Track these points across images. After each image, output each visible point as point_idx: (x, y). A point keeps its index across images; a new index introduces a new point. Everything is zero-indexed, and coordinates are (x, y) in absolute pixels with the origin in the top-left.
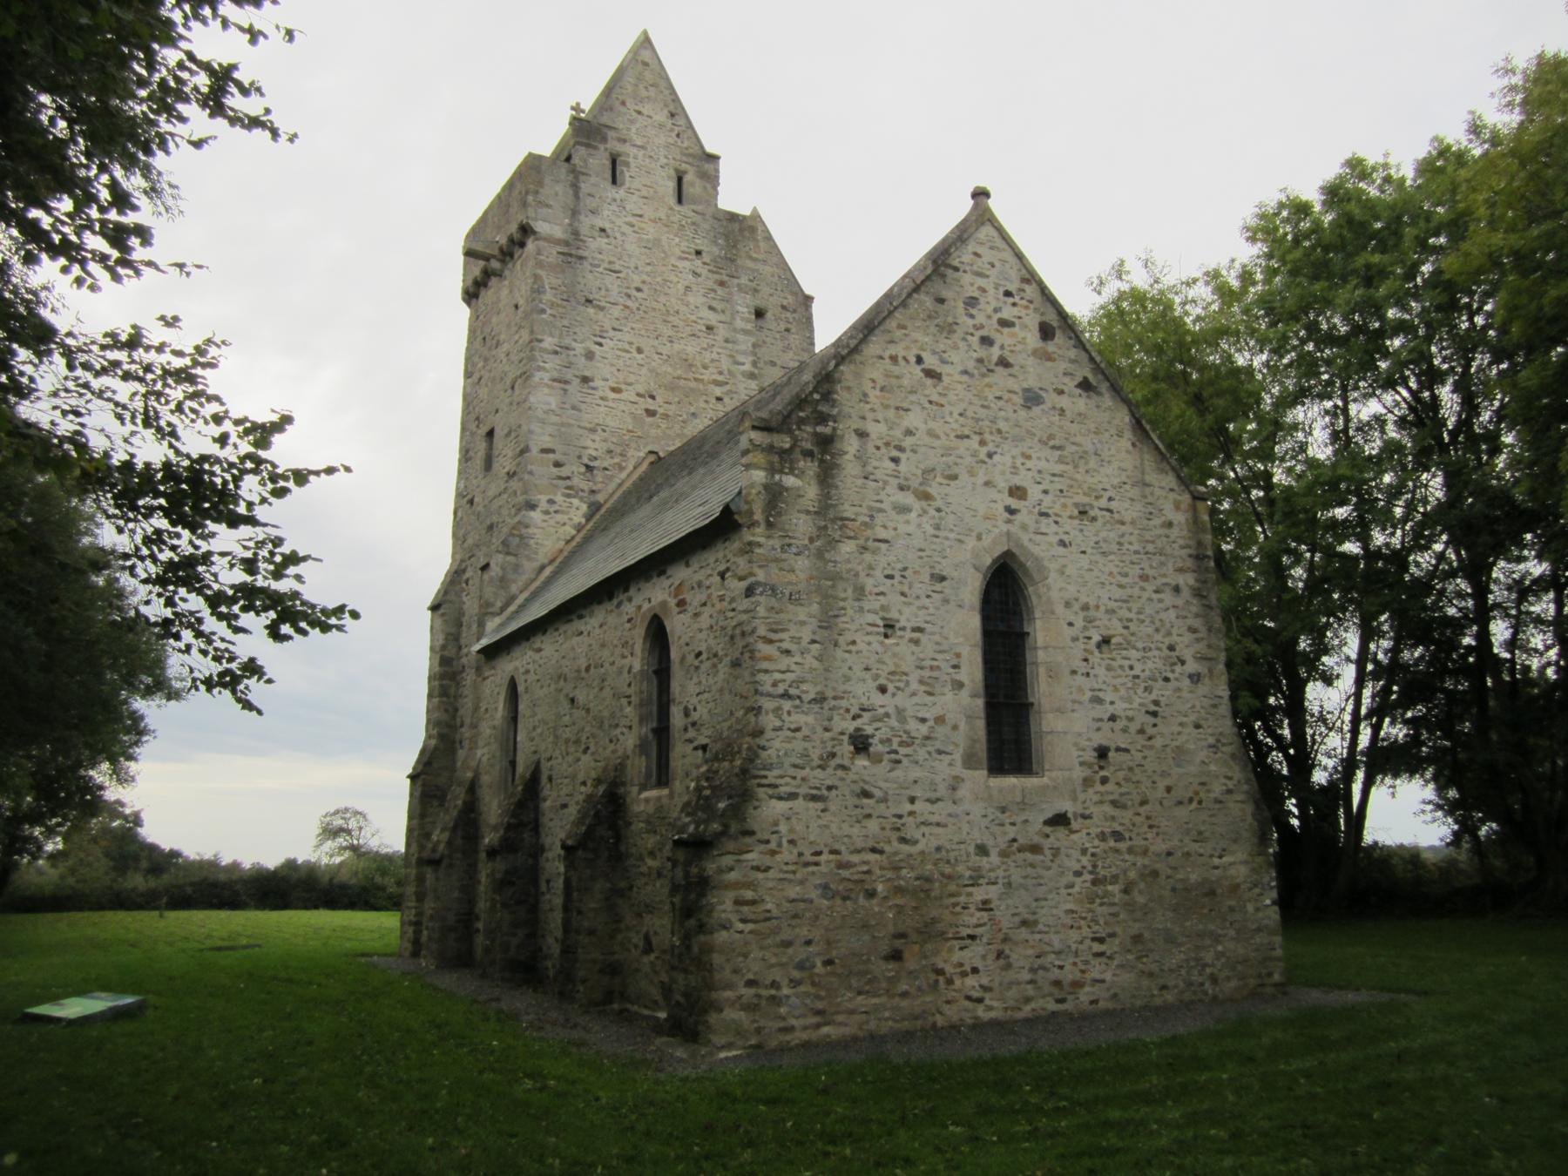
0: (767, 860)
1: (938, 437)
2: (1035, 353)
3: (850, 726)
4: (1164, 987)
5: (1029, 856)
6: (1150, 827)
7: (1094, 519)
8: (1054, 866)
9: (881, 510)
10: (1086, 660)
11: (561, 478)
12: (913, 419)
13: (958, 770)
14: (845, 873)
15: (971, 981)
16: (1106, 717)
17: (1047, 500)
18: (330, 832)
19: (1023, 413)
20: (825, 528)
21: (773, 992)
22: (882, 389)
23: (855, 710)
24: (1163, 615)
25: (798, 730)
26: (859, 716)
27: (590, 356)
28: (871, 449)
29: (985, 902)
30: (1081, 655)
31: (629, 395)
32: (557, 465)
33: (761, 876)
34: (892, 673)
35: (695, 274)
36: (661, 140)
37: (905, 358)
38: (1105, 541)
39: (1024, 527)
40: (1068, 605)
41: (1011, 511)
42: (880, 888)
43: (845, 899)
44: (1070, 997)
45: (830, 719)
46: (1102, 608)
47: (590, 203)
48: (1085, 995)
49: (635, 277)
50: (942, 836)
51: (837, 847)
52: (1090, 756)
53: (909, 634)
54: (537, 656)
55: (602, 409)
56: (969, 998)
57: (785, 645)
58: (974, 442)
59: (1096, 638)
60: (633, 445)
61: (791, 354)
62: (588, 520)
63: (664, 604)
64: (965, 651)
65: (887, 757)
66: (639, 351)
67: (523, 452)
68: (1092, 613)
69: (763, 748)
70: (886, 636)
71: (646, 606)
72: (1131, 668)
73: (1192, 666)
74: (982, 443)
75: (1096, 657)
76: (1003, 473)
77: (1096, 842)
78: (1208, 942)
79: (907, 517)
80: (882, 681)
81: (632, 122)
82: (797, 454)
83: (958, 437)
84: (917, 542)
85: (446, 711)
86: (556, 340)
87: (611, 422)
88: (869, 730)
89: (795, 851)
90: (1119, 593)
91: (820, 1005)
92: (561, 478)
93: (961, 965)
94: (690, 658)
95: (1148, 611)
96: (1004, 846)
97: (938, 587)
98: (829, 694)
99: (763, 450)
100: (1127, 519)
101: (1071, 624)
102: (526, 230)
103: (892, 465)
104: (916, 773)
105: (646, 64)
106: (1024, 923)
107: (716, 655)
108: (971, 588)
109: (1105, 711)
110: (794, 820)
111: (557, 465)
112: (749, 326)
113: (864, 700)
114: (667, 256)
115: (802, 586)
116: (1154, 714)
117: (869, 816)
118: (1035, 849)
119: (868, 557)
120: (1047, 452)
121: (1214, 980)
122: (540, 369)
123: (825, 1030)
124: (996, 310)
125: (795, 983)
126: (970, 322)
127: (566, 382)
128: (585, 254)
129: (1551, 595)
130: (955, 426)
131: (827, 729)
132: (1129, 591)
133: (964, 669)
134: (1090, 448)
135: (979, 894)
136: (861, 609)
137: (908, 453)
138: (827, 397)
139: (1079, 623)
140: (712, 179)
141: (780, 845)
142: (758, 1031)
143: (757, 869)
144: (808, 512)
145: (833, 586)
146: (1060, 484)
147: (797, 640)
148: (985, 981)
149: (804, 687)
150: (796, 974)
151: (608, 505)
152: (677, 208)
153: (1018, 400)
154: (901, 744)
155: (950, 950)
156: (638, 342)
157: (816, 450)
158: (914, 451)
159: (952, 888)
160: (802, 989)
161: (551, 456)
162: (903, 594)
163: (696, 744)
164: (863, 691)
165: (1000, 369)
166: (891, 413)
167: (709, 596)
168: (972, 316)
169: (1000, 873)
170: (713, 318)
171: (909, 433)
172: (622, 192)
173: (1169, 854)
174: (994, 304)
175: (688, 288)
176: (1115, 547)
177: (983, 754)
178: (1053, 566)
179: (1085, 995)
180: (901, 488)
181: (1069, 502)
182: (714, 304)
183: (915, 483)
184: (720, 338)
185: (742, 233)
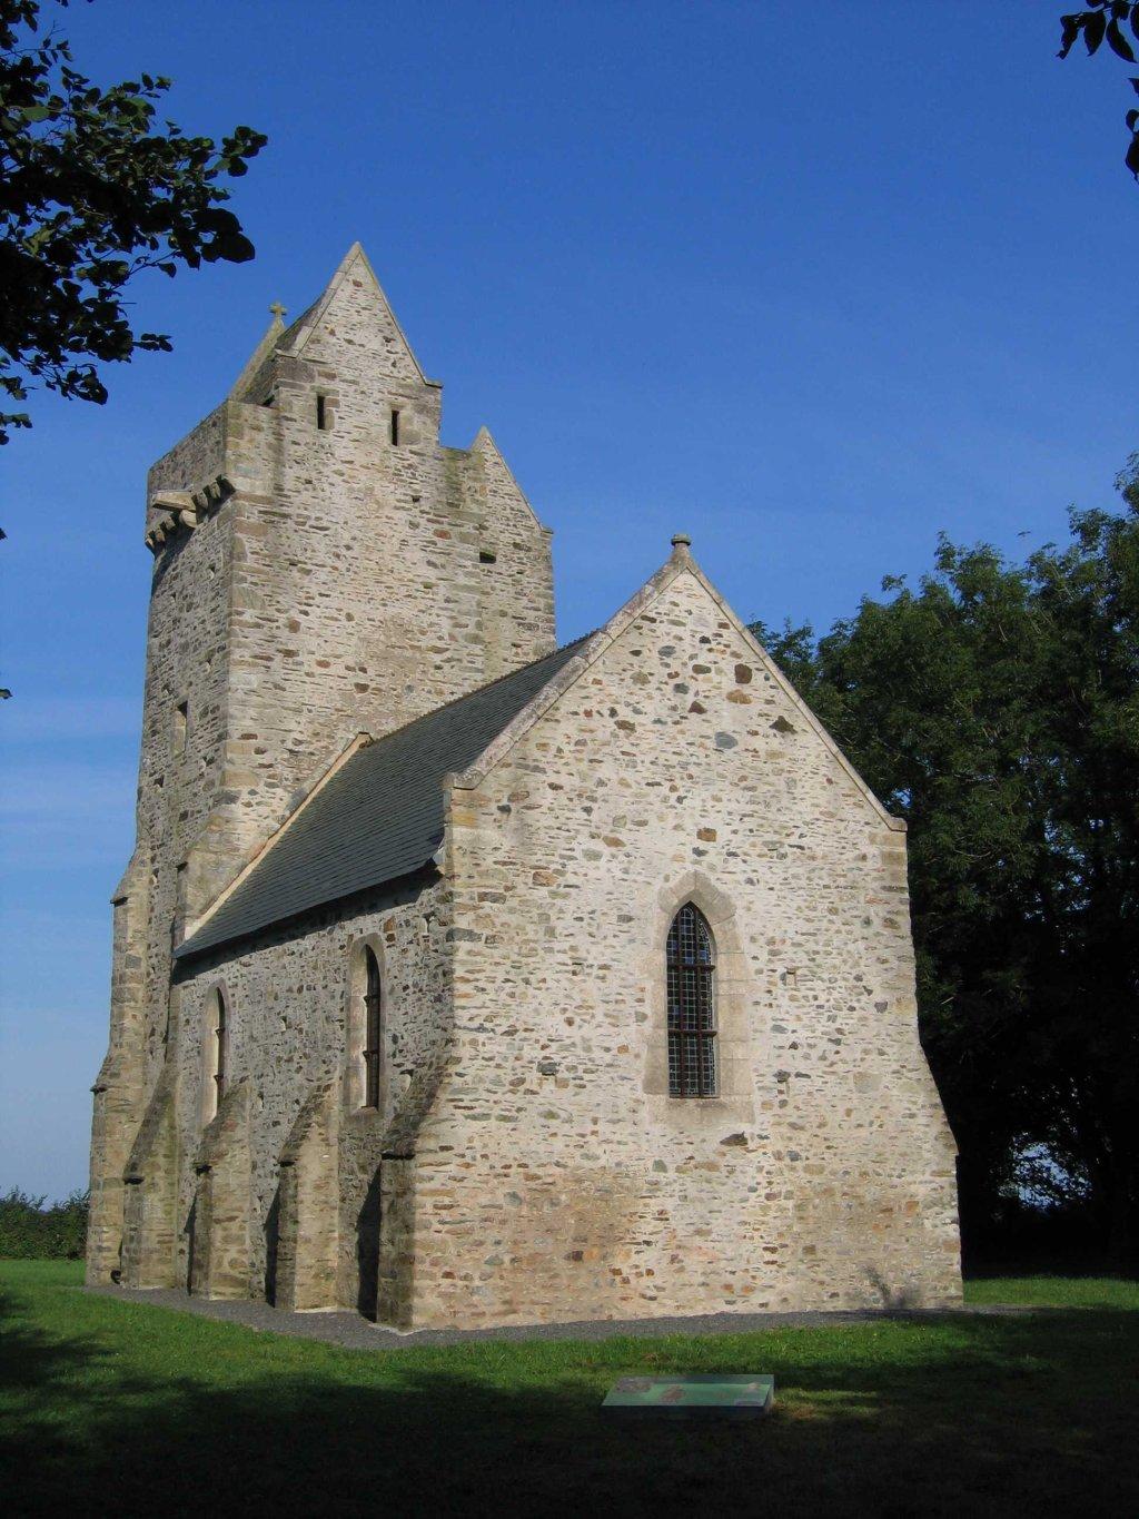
0: (463, 1172)
1: (629, 786)
5: (703, 1171)
6: (828, 1148)
7: (784, 856)
8: (730, 1182)
9: (571, 858)
10: (769, 992)
13: (640, 1094)
15: (646, 1281)
16: (788, 1045)
19: (714, 757)
23: (544, 1041)
24: (851, 947)
25: (491, 1059)
26: (547, 1047)
27: (294, 627)
30: (765, 986)
31: (337, 668)
32: (259, 751)
37: (598, 712)
38: (794, 876)
39: (712, 868)
40: (753, 939)
41: (699, 852)
42: (563, 1197)
44: (740, 1300)
45: (521, 1049)
46: (789, 942)
50: (623, 1153)
54: (244, 971)
55: (307, 687)
56: (644, 1296)
58: (665, 790)
59: (781, 970)
60: (342, 726)
61: (524, 601)
63: (374, 935)
64: (649, 985)
65: (572, 1082)
66: (350, 617)
67: (221, 738)
70: (574, 973)
71: (358, 936)
72: (816, 998)
73: (878, 997)
74: (673, 789)
75: (779, 990)
77: (772, 1161)
78: (310, 1105)
79: (596, 863)
80: (568, 1015)
83: (648, 784)
84: (607, 885)
86: (257, 612)
88: (556, 1059)
89: (488, 1164)
90: (808, 927)
92: (262, 766)
93: (637, 1267)
94: (399, 990)
95: (836, 943)
96: (680, 1163)
97: (625, 926)
98: (520, 1026)
101: (755, 958)
102: (227, 489)
103: (585, 815)
104: (600, 1097)
106: (698, 1232)
108: (655, 928)
116: (838, 1042)
117: (555, 1134)
118: (712, 1167)
119: (559, 902)
120: (738, 793)
122: (239, 646)
127: (269, 659)
130: (647, 774)
131: (517, 1059)
132: (816, 924)
135: (654, 1205)
137: (600, 803)
141: (474, 1159)
148: (659, 1282)
150: (488, 1269)
151: (313, 795)
152: (393, 449)
153: (711, 744)
155: (628, 1255)
162: (591, 935)
163: (403, 1068)
164: (554, 1024)
167: (416, 935)
168: (667, 665)
169: (676, 1187)
170: (431, 575)
171: (601, 783)
174: (690, 651)
176: (803, 882)
177: (665, 1080)
178: (740, 904)
180: (593, 836)
181: (759, 841)
182: (433, 558)
184: (440, 597)
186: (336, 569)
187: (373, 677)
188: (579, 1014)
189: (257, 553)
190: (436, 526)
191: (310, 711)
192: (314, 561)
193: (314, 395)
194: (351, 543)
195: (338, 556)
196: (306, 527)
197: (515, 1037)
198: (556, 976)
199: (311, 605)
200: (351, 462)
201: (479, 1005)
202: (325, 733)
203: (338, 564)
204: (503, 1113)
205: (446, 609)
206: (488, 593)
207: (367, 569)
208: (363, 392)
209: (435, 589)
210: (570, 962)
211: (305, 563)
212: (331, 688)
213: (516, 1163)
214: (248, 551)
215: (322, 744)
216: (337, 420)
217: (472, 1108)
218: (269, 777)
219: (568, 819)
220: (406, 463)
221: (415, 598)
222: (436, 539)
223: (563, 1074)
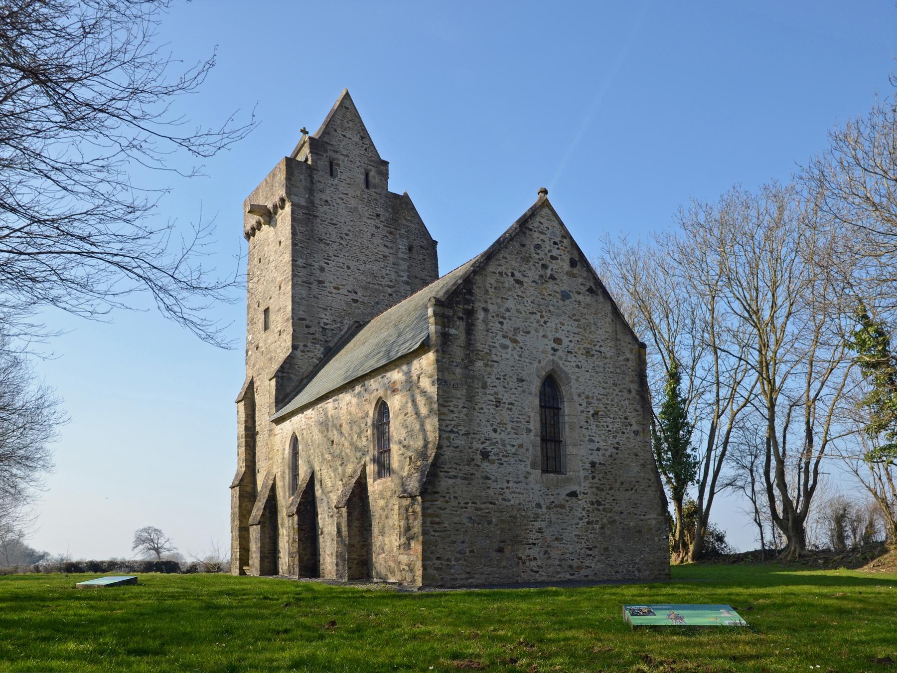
1: (521, 313)
2: (567, 273)
3: (481, 447)
4: (617, 572)
7: (593, 356)
9: (494, 347)
11: (309, 333)
12: (510, 304)
13: (529, 469)
14: (479, 513)
15: (533, 563)
17: (572, 345)
18: (140, 540)
19: (561, 303)
20: (469, 355)
22: (495, 288)
23: (483, 439)
27: (322, 269)
28: (490, 318)
29: (540, 529)
31: (343, 291)
32: (307, 327)
34: (499, 423)
35: (377, 227)
36: (357, 152)
39: (560, 358)
40: (579, 395)
43: (478, 524)
47: (320, 186)
48: (583, 572)
52: (588, 466)
53: (507, 406)
56: (532, 571)
57: (451, 408)
58: (538, 316)
59: (592, 412)
61: (426, 272)
64: (532, 414)
66: (348, 268)
68: (591, 400)
74: (542, 316)
75: (591, 421)
76: (551, 331)
81: (340, 141)
82: (455, 318)
84: (511, 362)
86: (304, 261)
88: (489, 449)
91: (468, 570)
92: (309, 333)
97: (520, 384)
98: (472, 432)
100: (608, 356)
101: (580, 405)
103: (500, 326)
104: (510, 469)
105: (347, 108)
106: (557, 539)
108: (535, 386)
109: (594, 446)
111: (307, 327)
112: (406, 257)
114: (361, 217)
115: (458, 381)
116: (617, 449)
117: (489, 488)
118: (562, 507)
119: (488, 369)
120: (572, 322)
121: (639, 570)
123: (471, 580)
124: (549, 251)
125: (457, 560)
126: (537, 257)
127: (310, 283)
128: (318, 214)
129: (849, 543)
132: (608, 391)
133: (532, 423)
134: (592, 321)
135: (537, 525)
136: (485, 394)
137: (507, 320)
139: (584, 404)
140: (385, 175)
141: (450, 498)
142: (442, 579)
143: (441, 509)
146: (578, 338)
147: (456, 406)
148: (539, 563)
149: (460, 428)
150: (458, 556)
154: (503, 456)
155: (525, 549)
158: (510, 319)
159: (525, 522)
160: (461, 562)
162: (504, 387)
164: (487, 430)
165: (550, 280)
166: (499, 301)
168: (538, 254)
169: (547, 516)
170: (386, 251)
171: (508, 310)
172: (336, 180)
173: (621, 513)
174: (548, 248)
176: (602, 370)
178: (573, 377)
179: (583, 572)
180: (504, 337)
181: (582, 347)
182: (387, 244)
183: (510, 335)
184: (390, 262)
185: (402, 204)
223: (492, 457)
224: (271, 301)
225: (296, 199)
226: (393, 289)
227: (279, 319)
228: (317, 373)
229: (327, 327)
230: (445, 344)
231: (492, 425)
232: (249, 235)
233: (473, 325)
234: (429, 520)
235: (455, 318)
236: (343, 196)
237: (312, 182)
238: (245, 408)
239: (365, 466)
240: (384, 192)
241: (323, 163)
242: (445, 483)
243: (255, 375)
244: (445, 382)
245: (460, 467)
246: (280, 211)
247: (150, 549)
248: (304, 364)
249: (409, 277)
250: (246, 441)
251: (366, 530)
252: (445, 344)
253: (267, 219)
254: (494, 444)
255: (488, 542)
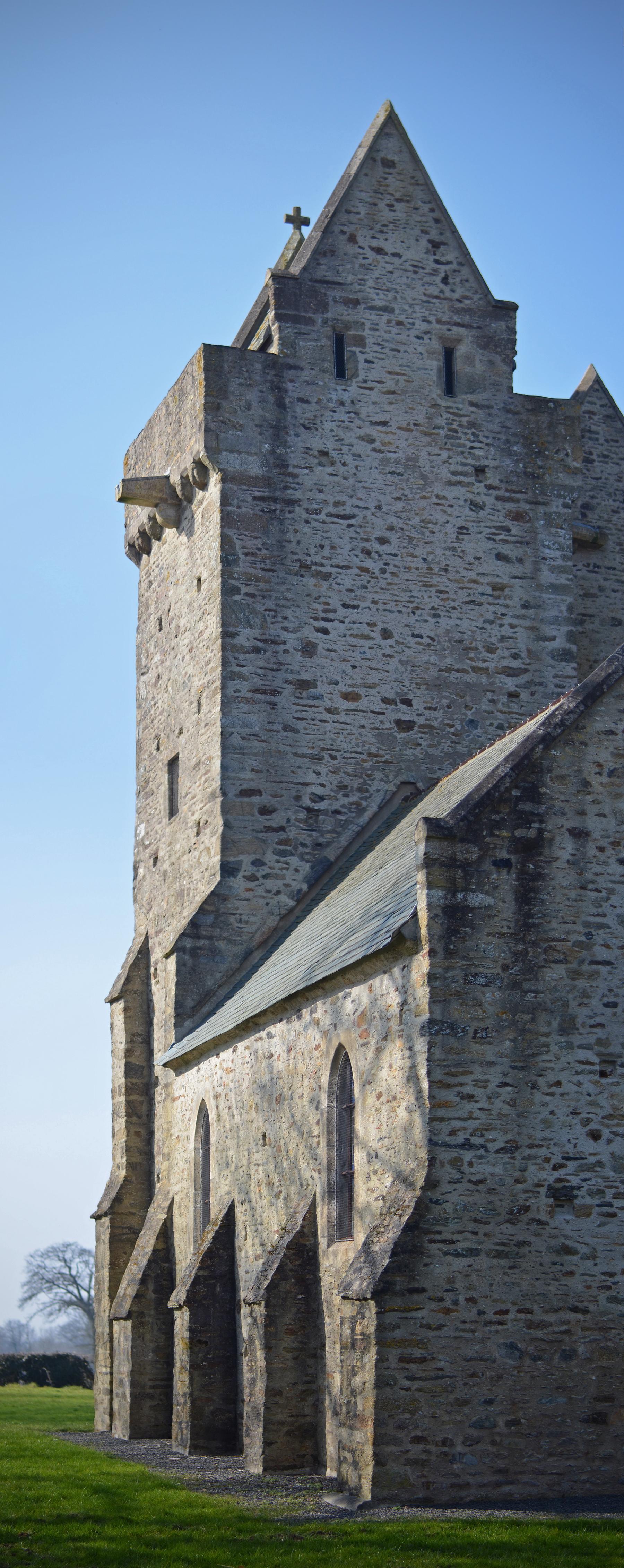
0: (441, 1318)
3: (550, 1177)
11: (268, 829)
20: (525, 953)
21: (445, 1449)
23: (556, 1159)
26: (562, 1166)
27: (309, 649)
32: (265, 811)
33: (432, 1334)
35: (476, 506)
42: (581, 1349)
43: (535, 1359)
45: (523, 1170)
49: (379, 522)
51: (528, 1305)
55: (328, 726)
57: (466, 1090)
60: (379, 775)
62: (311, 887)
66: (386, 634)
69: (437, 1202)
70: (603, 1074)
80: (593, 1126)
81: (367, 268)
82: (487, 866)
85: (137, 1134)
86: (257, 633)
87: (342, 743)
88: (575, 1181)
89: (474, 1310)
91: (501, 1464)
92: (268, 829)
98: (524, 1141)
99: (442, 865)
107: (395, 1098)
110: (474, 1277)
111: (265, 811)
113: (569, 1148)
115: (489, 1023)
117: (571, 1273)
119: (581, 983)
123: (507, 1488)
128: (298, 495)
131: (518, 1181)
138: (533, 794)
141: (456, 1302)
142: (427, 1485)
143: (429, 1327)
144: (501, 935)
145: (533, 1020)
149: (490, 1135)
150: (474, 1433)
156: (384, 620)
157: (513, 858)
160: (480, 1447)
161: (256, 799)
170: (503, 571)
172: (353, 388)
175: (462, 530)
182: (506, 550)
184: (515, 602)
186: (366, 570)
187: (422, 710)
188: (608, 1126)
189: (253, 554)
190: (509, 506)
191: (333, 758)
192: (334, 562)
193: (328, 330)
194: (387, 534)
195: (368, 553)
196: (322, 517)
197: (516, 1154)
198: (576, 1078)
199: (331, 621)
200: (384, 423)
201: (464, 1116)
202: (355, 786)
203: (368, 564)
204: (497, 1248)
205: (524, 617)
206: (594, 596)
207: (409, 568)
208: (400, 323)
209: (507, 592)
210: (596, 1060)
211: (322, 565)
212: (363, 727)
213: (516, 1308)
214: (240, 552)
215: (353, 799)
216: (362, 365)
217: (452, 1242)
218: (280, 843)
219: (597, 875)
220: (465, 420)
221: (480, 604)
222: (508, 523)
223: (583, 1199)
224: (183, 739)
225: (234, 462)
226: (522, 679)
227: (197, 790)
228: (288, 932)
229: (322, 806)
230: (455, 932)
231: (586, 1122)
232: (139, 549)
233: (539, 876)
234: (394, 1354)
235: (487, 866)
236: (374, 432)
237: (281, 405)
238: (127, 1019)
239: (313, 1205)
240: (503, 396)
241: (315, 344)
242: (440, 1269)
243: (152, 932)
244: (452, 1027)
245: (488, 1228)
246: (199, 494)
247: (69, 1303)
248: (252, 912)
249: (571, 637)
250: (128, 1102)
251: (315, 1356)
252: (455, 932)
253: (171, 512)
254: (590, 1168)
255: (562, 1400)
